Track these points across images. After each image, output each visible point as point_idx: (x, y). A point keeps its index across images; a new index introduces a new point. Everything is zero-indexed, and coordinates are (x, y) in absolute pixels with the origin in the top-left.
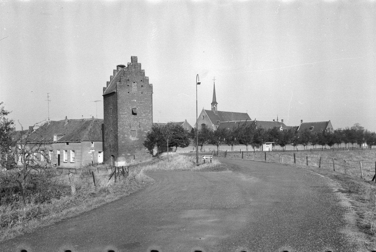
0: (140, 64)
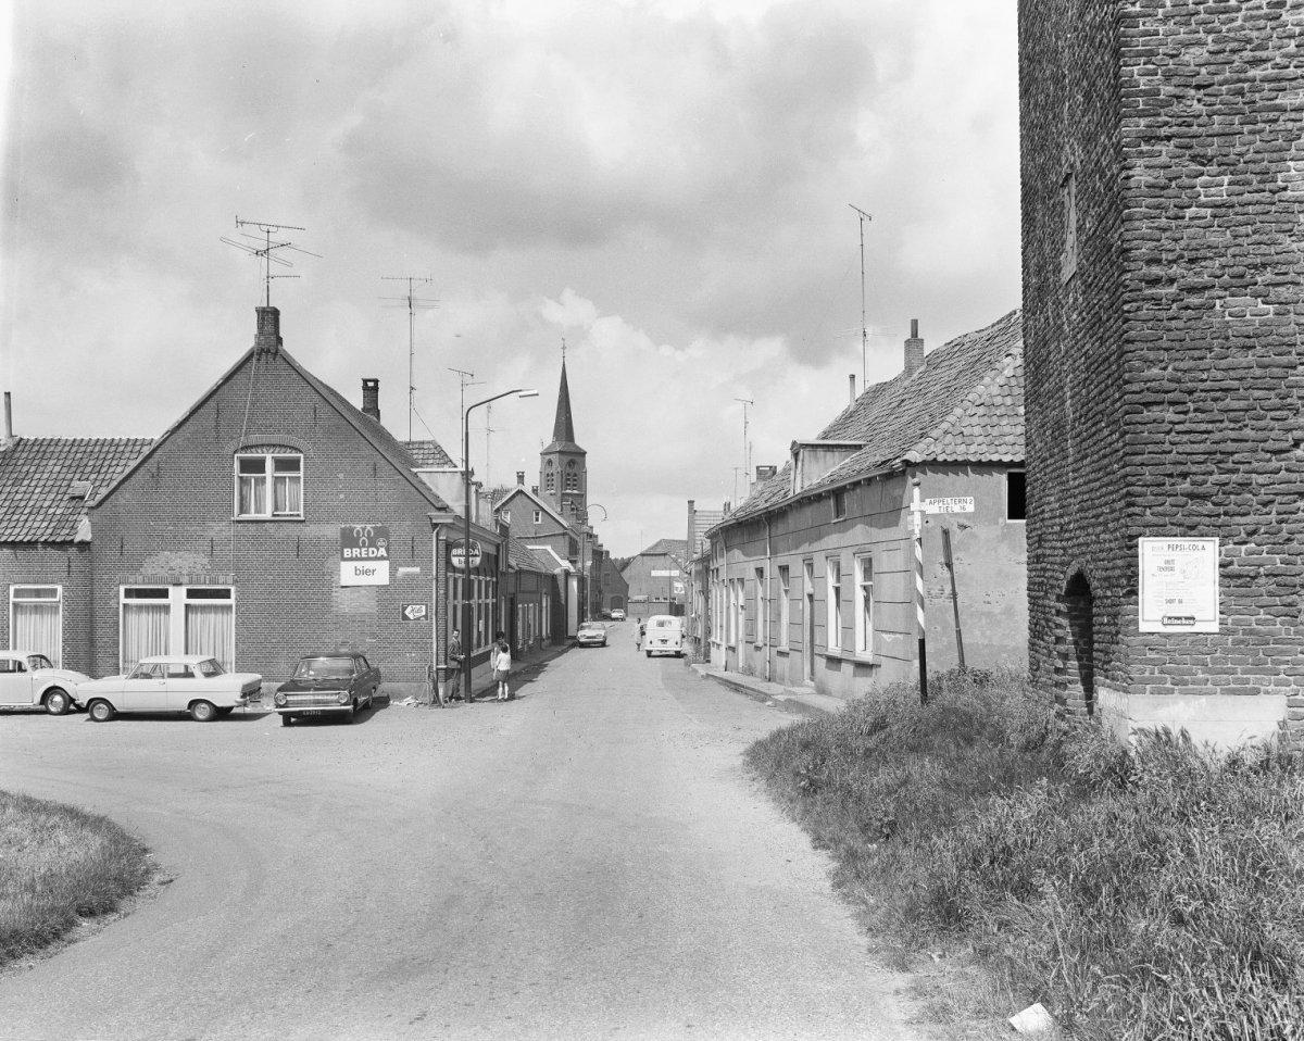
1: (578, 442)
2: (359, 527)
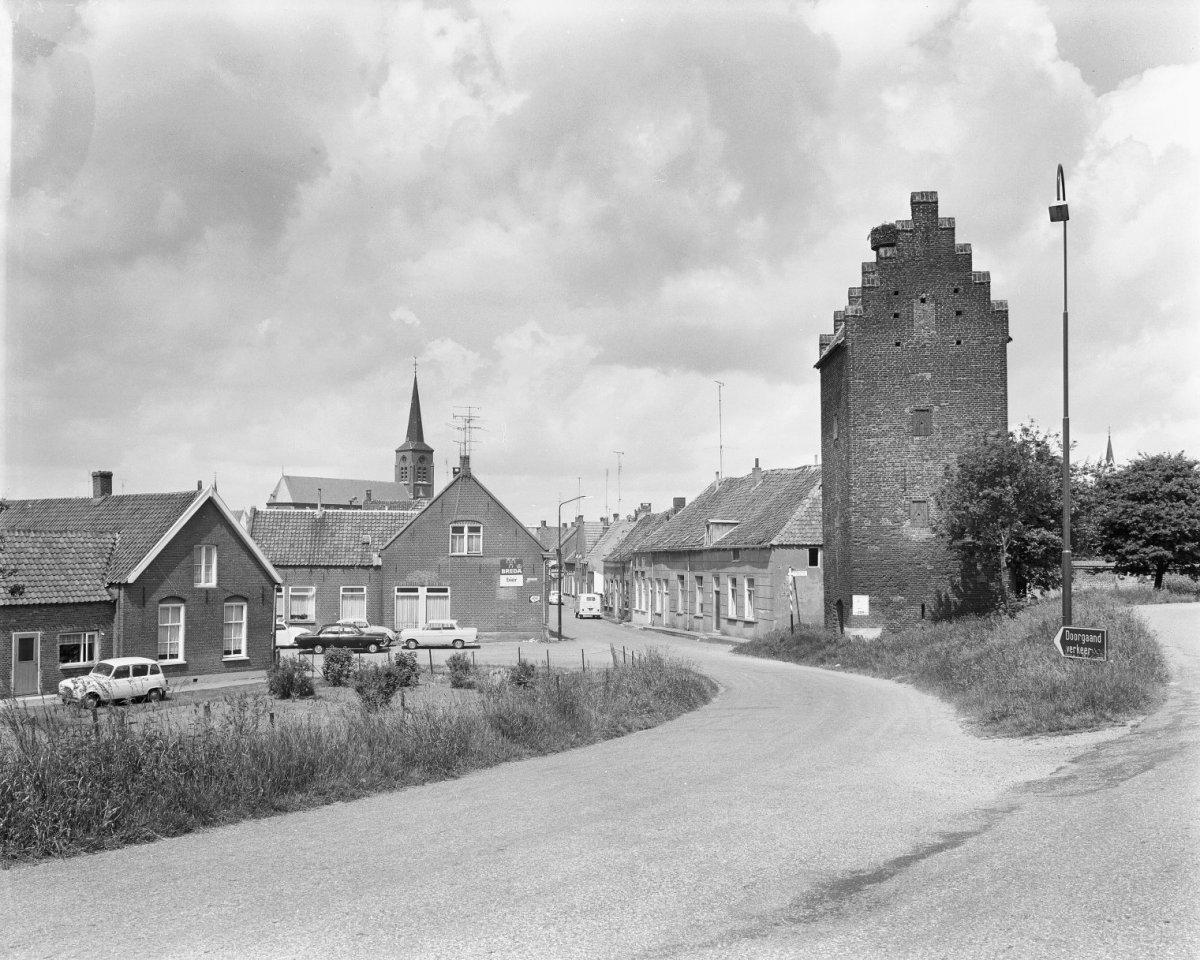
0: (951, 220)
1: (427, 441)
2: (508, 559)
